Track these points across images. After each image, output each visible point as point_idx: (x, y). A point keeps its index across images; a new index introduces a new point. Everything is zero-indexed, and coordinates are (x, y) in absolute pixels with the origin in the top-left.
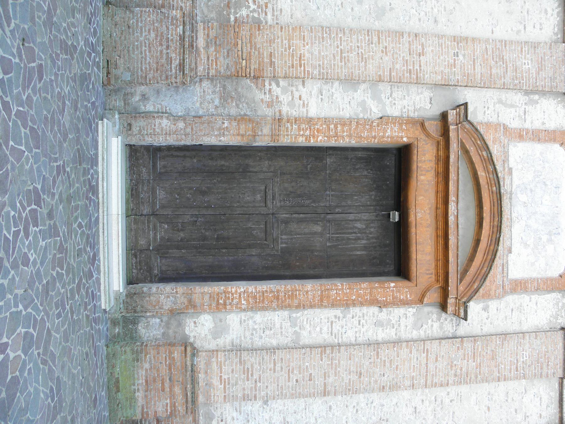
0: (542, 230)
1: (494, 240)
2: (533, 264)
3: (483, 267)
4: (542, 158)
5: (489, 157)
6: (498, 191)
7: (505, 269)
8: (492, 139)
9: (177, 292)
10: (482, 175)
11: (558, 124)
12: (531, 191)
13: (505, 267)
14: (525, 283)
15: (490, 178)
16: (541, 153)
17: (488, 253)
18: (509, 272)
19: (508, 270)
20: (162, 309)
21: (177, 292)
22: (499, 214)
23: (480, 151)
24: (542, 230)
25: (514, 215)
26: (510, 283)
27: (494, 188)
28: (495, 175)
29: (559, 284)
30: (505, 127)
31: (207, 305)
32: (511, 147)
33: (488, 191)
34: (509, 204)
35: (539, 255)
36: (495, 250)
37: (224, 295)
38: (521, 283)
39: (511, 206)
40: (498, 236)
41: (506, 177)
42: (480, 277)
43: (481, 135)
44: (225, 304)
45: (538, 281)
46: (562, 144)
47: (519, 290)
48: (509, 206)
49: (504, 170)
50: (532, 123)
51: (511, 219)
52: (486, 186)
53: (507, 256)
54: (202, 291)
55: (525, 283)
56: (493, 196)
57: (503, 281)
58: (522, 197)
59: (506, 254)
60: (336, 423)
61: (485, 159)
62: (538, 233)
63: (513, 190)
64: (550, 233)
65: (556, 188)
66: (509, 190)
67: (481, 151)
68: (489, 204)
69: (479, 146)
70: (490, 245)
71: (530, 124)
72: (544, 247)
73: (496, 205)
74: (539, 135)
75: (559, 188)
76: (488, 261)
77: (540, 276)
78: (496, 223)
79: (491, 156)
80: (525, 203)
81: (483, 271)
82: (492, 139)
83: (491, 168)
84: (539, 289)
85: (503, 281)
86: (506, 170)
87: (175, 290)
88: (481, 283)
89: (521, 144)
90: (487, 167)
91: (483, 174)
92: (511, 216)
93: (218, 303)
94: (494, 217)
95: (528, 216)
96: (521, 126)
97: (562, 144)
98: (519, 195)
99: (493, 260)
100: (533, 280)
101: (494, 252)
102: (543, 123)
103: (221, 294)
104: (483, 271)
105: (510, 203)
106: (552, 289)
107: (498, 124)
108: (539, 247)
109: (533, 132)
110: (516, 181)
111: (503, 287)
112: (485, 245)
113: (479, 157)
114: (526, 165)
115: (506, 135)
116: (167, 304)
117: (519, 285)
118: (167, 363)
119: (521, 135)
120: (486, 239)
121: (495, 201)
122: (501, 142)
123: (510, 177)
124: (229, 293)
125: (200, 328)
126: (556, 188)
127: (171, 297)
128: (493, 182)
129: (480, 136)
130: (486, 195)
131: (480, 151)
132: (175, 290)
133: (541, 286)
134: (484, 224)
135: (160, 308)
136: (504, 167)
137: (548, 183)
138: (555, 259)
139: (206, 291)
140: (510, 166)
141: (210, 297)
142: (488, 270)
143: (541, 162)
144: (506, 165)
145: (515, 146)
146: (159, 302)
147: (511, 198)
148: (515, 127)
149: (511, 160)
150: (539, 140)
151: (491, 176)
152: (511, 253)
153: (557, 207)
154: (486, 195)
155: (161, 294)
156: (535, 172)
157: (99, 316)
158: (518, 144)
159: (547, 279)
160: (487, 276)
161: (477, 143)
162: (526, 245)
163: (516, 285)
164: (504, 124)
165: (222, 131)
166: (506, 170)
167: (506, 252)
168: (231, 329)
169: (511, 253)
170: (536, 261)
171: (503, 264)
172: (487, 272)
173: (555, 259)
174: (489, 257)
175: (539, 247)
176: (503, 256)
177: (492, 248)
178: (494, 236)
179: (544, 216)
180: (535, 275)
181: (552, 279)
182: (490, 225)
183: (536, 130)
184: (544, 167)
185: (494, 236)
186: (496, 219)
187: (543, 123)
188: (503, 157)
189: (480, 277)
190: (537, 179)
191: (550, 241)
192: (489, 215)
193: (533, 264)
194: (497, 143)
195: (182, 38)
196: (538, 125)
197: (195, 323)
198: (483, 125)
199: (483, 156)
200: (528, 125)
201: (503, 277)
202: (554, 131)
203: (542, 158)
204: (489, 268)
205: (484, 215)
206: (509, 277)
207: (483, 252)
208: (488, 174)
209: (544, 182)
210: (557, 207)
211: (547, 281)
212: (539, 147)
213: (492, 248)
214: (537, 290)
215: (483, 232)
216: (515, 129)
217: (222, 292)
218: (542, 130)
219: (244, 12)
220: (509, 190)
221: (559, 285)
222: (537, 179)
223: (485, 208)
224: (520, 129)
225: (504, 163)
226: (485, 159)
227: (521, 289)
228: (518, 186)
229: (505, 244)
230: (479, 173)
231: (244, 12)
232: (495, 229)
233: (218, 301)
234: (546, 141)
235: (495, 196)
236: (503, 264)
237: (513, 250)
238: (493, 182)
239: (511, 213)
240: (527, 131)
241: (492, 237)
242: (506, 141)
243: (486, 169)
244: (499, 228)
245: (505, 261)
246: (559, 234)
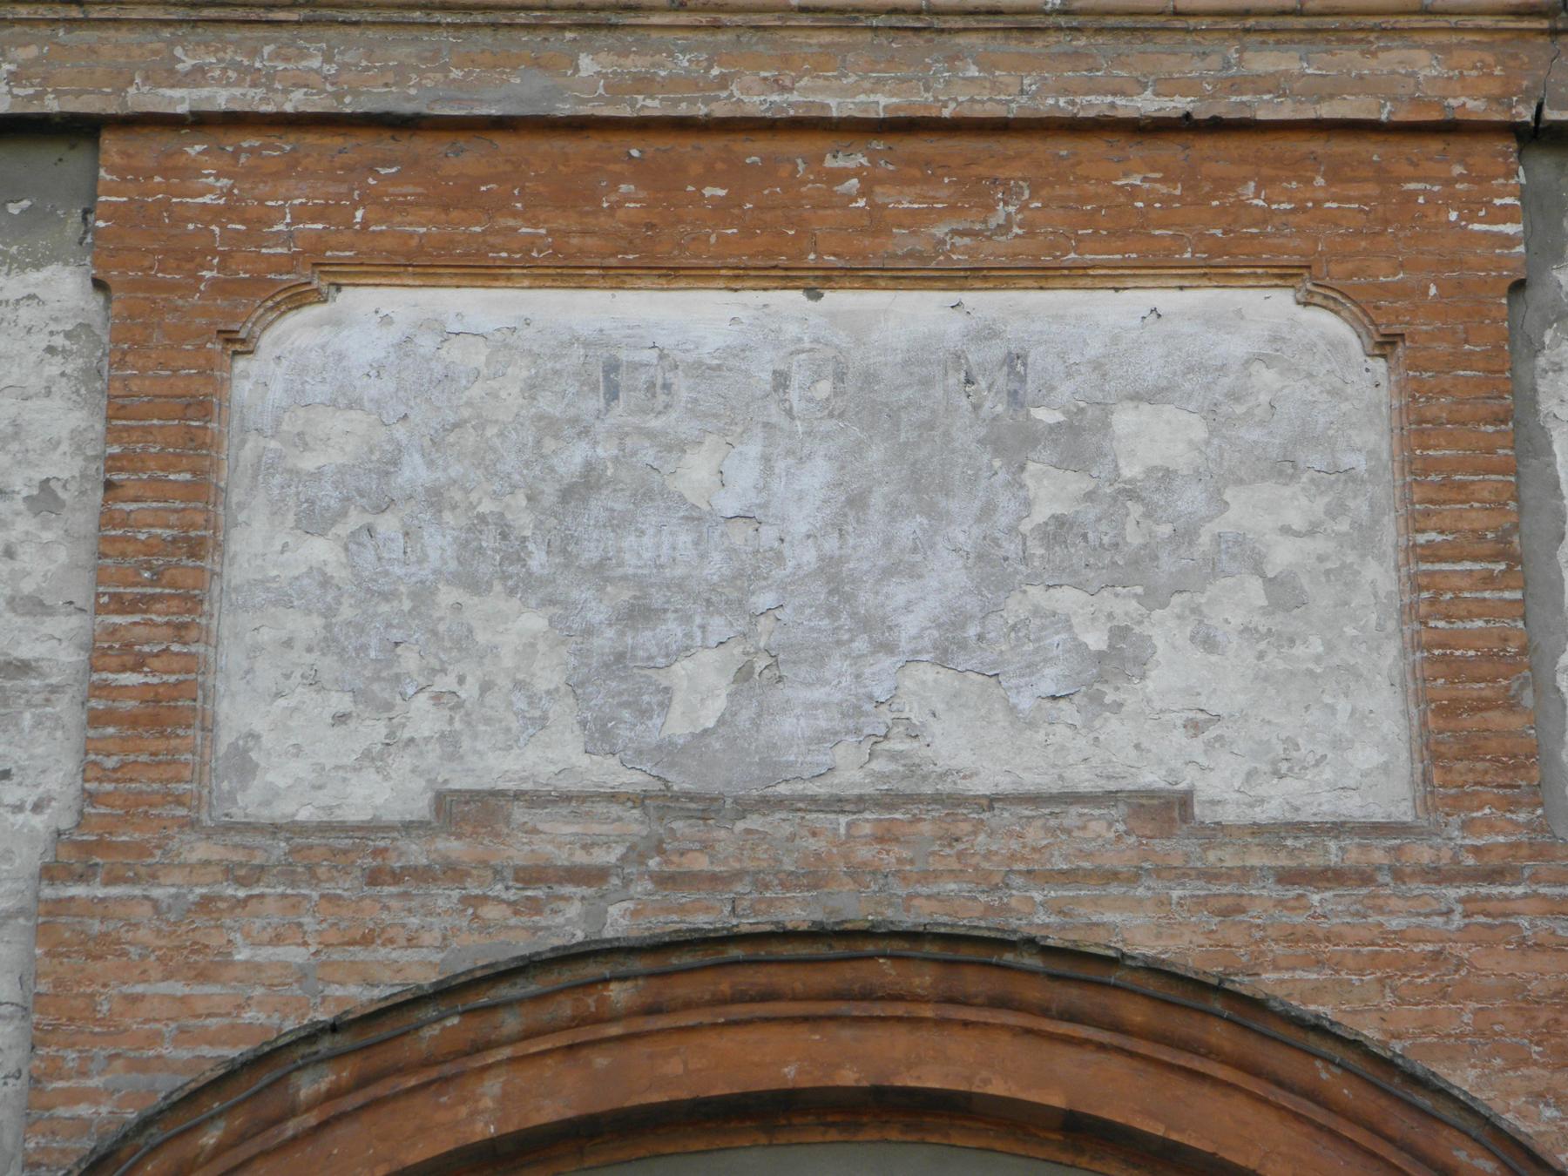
0: (988, 511)
1: (1072, 996)
2: (1284, 593)
3: (1312, 1095)
4: (355, 520)
5: (342, 1041)
6: (638, 964)
7: (1333, 853)
8: (178, 988)
10: (504, 1098)
11: (53, 368)
12: (638, 614)
13: (1311, 861)
14: (1454, 669)
15: (528, 1035)
16: (313, 521)
17: (1185, 1046)
18: (1353, 808)
19: (1338, 829)
22: (840, 949)
23: (291, 1128)
24: (988, 511)
25: (852, 771)
26: (1455, 804)
27: (619, 994)
28: (505, 991)
29: (1459, 360)
30: (73, 857)
32: (248, 804)
33: (640, 1049)
34: (754, 822)
35: (1205, 539)
36: (1152, 985)
38: (1449, 710)
39: (768, 804)
40: (1031, 961)
41: (518, 852)
42: (1401, 1123)
43: (145, 1123)
45: (1431, 553)
46: (228, 337)
47: (1515, 722)
48: (777, 824)
49: (453, 872)
50: (35, 606)
51: (889, 801)
52: (600, 1061)
53: (1217, 833)
55: (1454, 669)
56: (688, 1005)
57: (1437, 875)
58: (699, 694)
59: (1192, 845)
61: (362, 1082)
62: (1011, 548)
63: (633, 780)
64: (1014, 443)
65: (613, 394)
66: (634, 824)
67: (293, 1112)
68: (750, 1035)
69: (241, 1138)
70: (1117, 1027)
71: (50, 625)
72: (1131, 493)
73: (760, 978)
74: (150, 548)
75: (612, 367)
76: (1251, 1047)
77: (1390, 532)
78: (923, 979)
79: (334, 1028)
80: (744, 674)
81: (1347, 1092)
82: (178, 988)
83: (439, 1030)
84: (1503, 537)
85: (1437, 875)
86: (453, 847)
88: (1447, 1112)
89: (224, 708)
90: (427, 1063)
91: (491, 1088)
92: (861, 803)
94: (867, 996)
95: (861, 644)
96: (66, 709)
97: (228, 337)
98: (677, 725)
99: (1251, 1010)
100: (1425, 600)
101: (1175, 994)
102: (45, 499)
104: (1347, 1092)
105: (744, 808)
106: (1498, 420)
107: (43, 931)
108: (1134, 538)
109: (120, 604)
110: (558, 755)
111: (1494, 875)
112: (1116, 1066)
113: (343, 1131)
114: (409, 661)
115: (142, 850)
117: (1469, 722)
119: (148, 709)
120: (1066, 1061)
121: (724, 984)
122: (205, 903)
123: (519, 813)
126: (613, 394)
128: (565, 1008)
129: (156, 1133)
130: (674, 1067)
131: (291, 1128)
133: (1477, 518)
134: (931, 1079)
136: (423, 875)
137: (572, 458)
138: (1235, 396)
140: (421, 807)
142: (1339, 1053)
143: (388, 525)
144: (415, 852)
145: (244, 767)
147: (706, 807)
148: (70, 765)
149: (373, 796)
150: (195, 548)
151: (511, 1023)
152: (1184, 801)
153: (781, 380)
154: (674, 1067)
156: (475, 586)
158: (225, 739)
159: (1415, 467)
160: (1388, 1064)
161: (219, 1150)
162: (1123, 657)
163: (1471, 751)
164: (49, 873)
165: (315, 105)
166: (453, 847)
167: (1177, 848)
169: (1184, 801)
170: (1258, 569)
171: (1287, 877)
172: (1353, 1059)
173: (1235, 396)
174: (1219, 1034)
175: (1134, 538)
176: (1210, 876)
177: (1136, 1013)
178: (1033, 992)
179: (857, 502)
180: (1380, 577)
181: (1416, 427)
182: (941, 1023)
183: (101, 577)
184: (435, 499)
185: (1033, 992)
186: (887, 973)
187: (45, 499)
188: (344, 887)
189: (1401, 1123)
190: (538, 560)
191: (1078, 441)
192: (847, 1034)
193: (1284, 593)
194: (216, 940)
196: (62, 555)
198: (56, 1072)
199: (332, 1095)
200: (57, 645)
201: (1398, 875)
202: (119, 410)
203: (355, 520)
204: (1313, 1041)
205: (848, 1077)
206: (1404, 812)
207: (1181, 1088)
208: (489, 1045)
209: (566, 494)
210: (781, 380)
211: (1429, 466)
212: (263, 547)
213: (1136, 1013)
214: (1513, 559)
215: (997, 1088)
216: (88, 769)
218: (107, 519)
220: (634, 824)
221: (1467, 361)
222: (538, 560)
223: (791, 1074)
224: (95, 719)
225: (396, 877)
226: (362, 1082)
227: (1511, 705)
228: (600, 737)
229: (1111, 861)
230: (485, 1129)
232: (974, 982)
234: (203, 489)
235: (683, 989)
236: (1287, 877)
237: (1151, 778)
238: (565, 1008)
239: (836, 804)
240: (107, 653)
241: (1044, 1012)
242: (201, 850)
243: (451, 1070)
244: (966, 953)
245: (1257, 859)
246: (1014, 361)
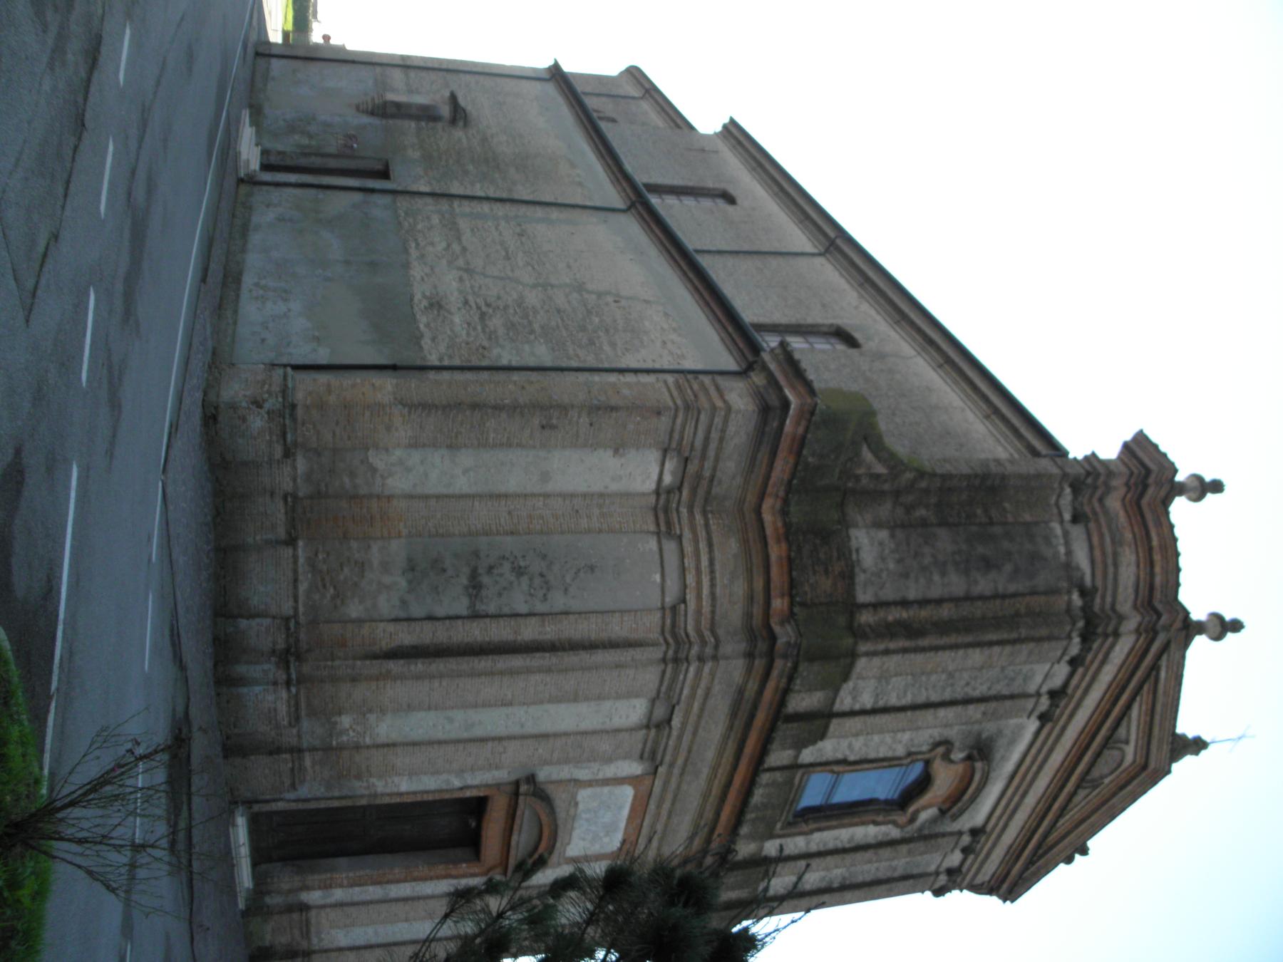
116: (285, 887)
125: (314, 897)
195: (292, 770)
219: (345, 738)
231: (345, 738)
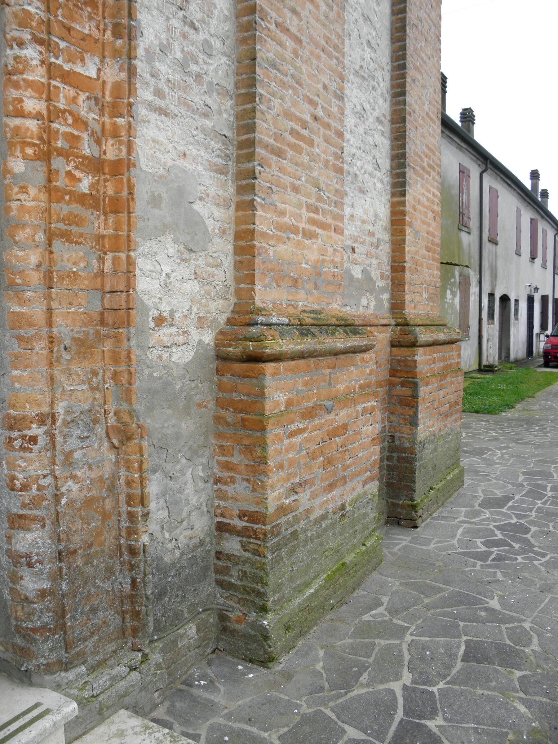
9: (41, 420)
20: (114, 478)
21: (41, 420)
31: (101, 260)
37: (58, 163)
44: (96, 165)
54: (35, 278)
60: (557, 549)
87: (35, 430)
93: (91, 200)
103: (51, 175)
118: (301, 426)
124: (48, 135)
127: (73, 443)
132: (35, 430)
135: (112, 488)
139: (34, 258)
141: (66, 236)
146: (89, 502)
155: (57, 497)
157: (483, 491)
168: (181, 163)
197: (160, 321)
217: (40, 166)
233: (81, 199)
